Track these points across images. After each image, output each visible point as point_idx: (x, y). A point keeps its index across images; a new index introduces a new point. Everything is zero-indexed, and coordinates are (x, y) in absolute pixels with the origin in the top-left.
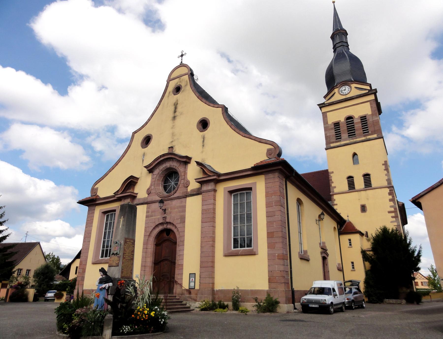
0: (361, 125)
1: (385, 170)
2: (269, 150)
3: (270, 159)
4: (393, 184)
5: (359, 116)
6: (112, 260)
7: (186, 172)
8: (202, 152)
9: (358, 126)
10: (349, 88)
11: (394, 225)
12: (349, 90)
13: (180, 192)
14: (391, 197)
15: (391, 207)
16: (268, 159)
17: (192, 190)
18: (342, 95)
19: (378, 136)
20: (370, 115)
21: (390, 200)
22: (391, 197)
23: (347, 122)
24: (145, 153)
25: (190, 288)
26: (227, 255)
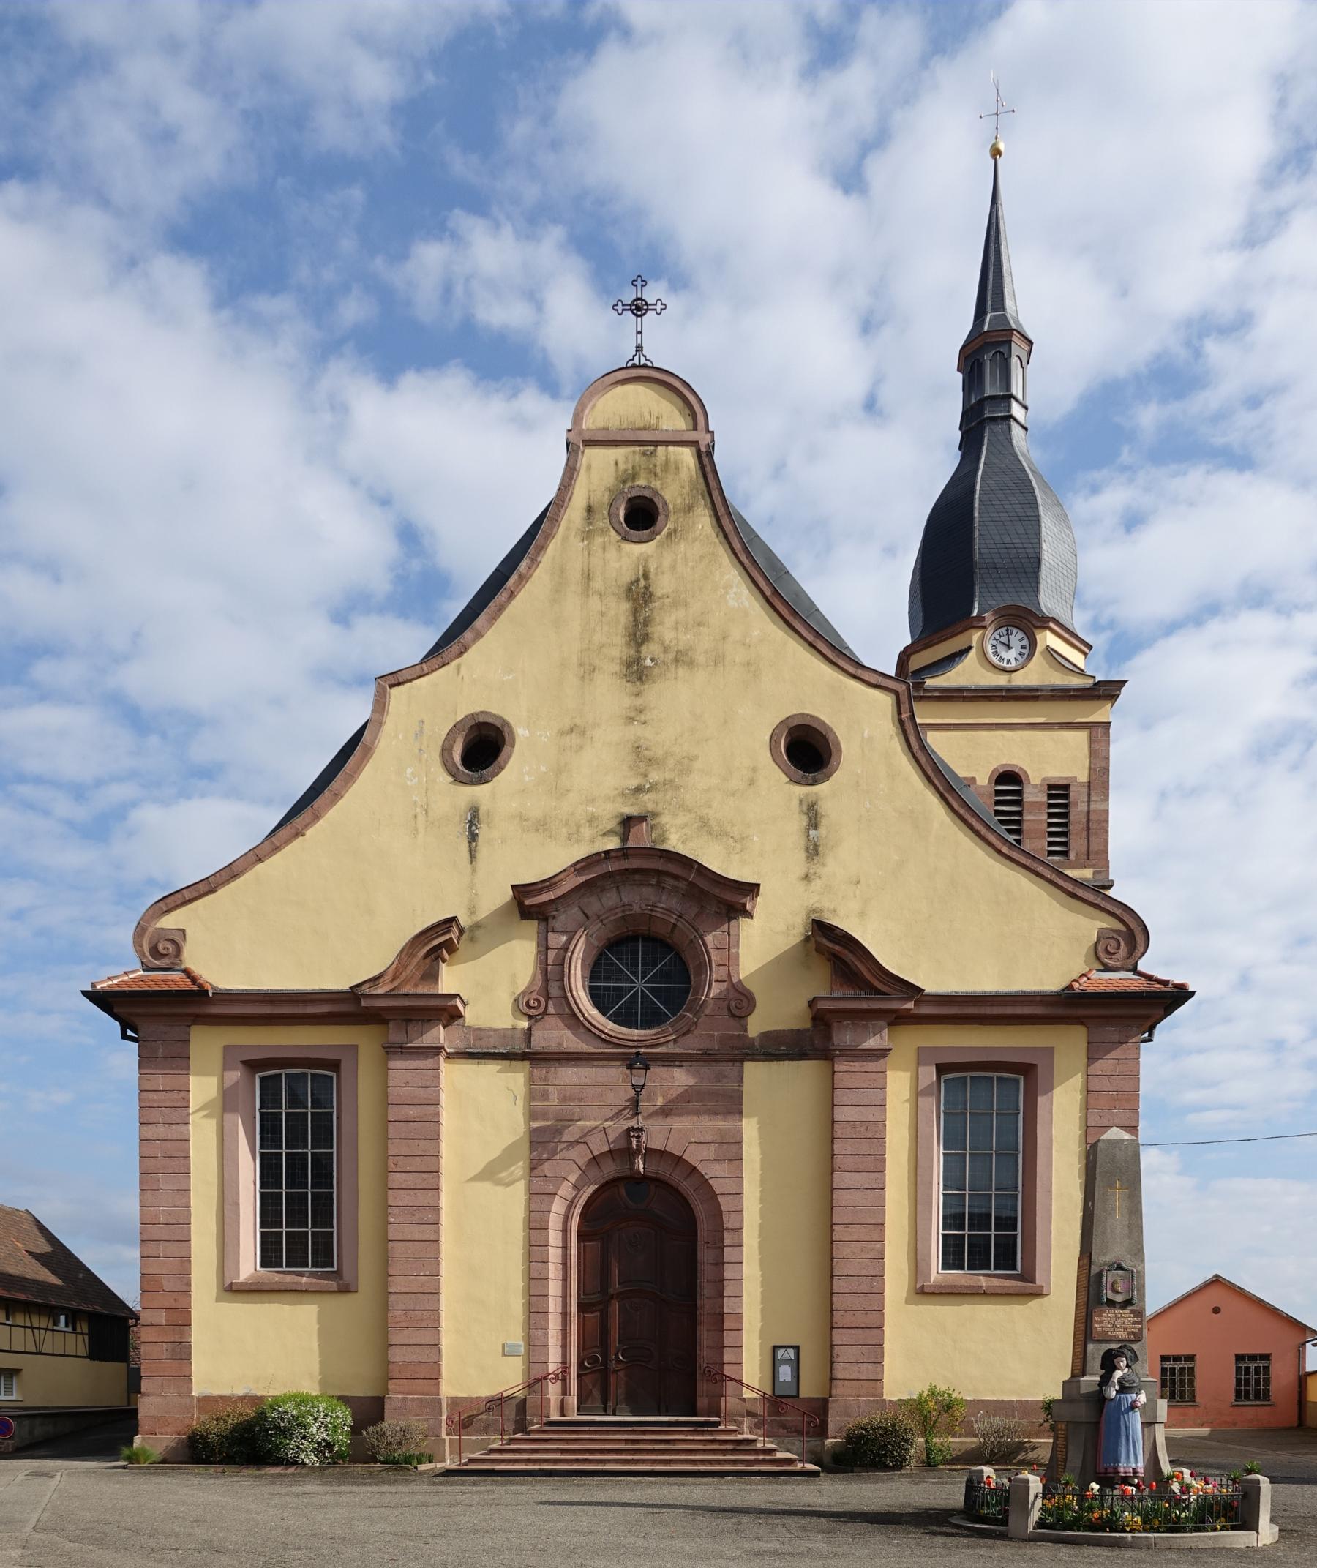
0: (1045, 817)
2: (1102, 935)
3: (1107, 969)
5: (1044, 779)
7: (733, 950)
8: (806, 877)
9: (1036, 819)
10: (1025, 642)
12: (1023, 651)
13: (713, 1036)
17: (766, 1036)
18: (995, 667)
19: (1099, 877)
20: (1081, 785)
23: (998, 793)
24: (482, 811)
26: (923, 1292)
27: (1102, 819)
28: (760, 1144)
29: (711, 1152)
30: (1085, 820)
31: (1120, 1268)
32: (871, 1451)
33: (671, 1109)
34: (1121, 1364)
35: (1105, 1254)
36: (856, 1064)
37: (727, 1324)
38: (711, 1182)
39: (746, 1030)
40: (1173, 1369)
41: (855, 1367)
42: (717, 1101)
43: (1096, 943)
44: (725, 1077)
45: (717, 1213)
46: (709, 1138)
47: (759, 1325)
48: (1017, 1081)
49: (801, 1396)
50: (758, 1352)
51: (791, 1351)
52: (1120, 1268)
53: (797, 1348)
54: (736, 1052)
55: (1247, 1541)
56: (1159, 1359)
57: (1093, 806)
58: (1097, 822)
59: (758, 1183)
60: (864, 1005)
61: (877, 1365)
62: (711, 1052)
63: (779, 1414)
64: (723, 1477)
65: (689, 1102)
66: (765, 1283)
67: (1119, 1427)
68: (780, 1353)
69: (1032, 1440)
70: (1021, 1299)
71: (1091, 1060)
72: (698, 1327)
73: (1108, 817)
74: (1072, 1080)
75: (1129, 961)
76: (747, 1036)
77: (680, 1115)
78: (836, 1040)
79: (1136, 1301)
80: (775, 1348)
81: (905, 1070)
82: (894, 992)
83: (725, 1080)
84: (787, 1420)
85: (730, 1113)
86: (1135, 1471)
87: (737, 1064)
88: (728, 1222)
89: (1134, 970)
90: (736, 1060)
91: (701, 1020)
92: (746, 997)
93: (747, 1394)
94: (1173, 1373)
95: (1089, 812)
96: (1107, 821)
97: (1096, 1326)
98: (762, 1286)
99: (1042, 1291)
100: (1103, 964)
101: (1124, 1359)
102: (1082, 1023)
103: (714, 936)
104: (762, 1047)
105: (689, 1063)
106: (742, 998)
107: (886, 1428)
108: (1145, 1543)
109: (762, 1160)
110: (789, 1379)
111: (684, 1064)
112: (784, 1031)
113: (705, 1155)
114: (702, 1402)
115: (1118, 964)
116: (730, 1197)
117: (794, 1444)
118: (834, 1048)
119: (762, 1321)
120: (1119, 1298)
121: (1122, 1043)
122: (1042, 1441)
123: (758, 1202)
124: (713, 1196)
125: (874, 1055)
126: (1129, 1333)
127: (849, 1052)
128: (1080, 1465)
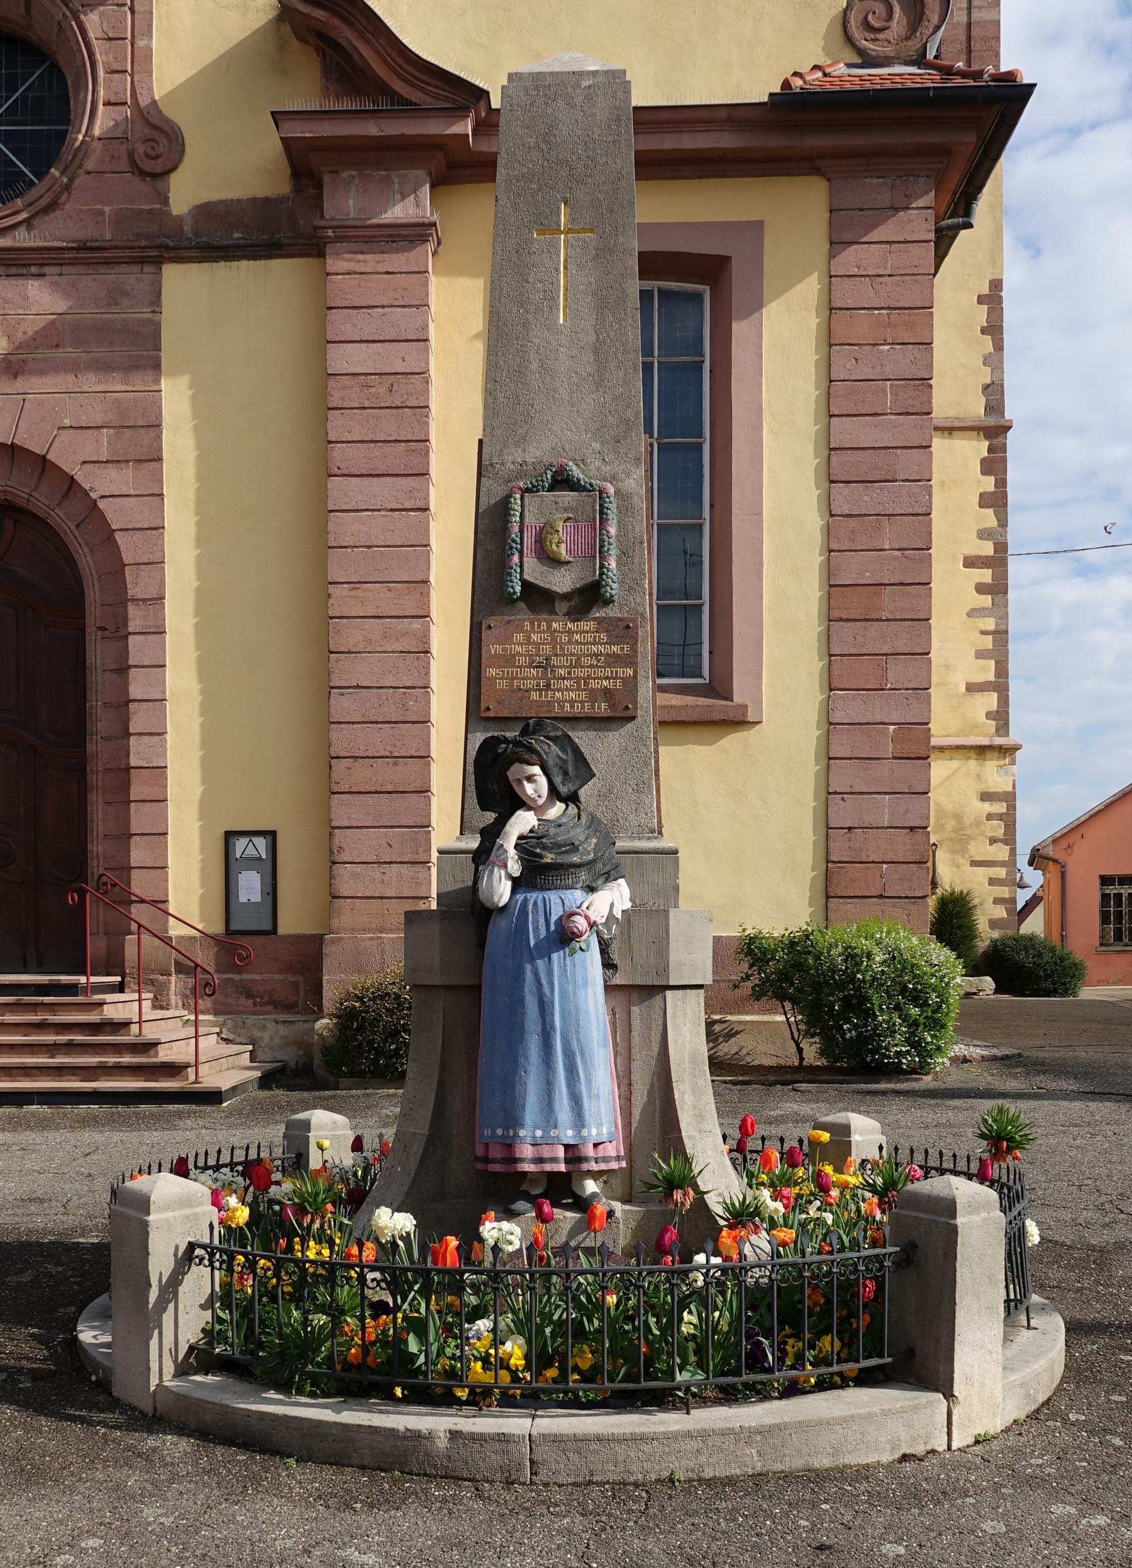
1: (984, 331)
3: (868, 61)
4: (1012, 411)
6: (522, 661)
7: (141, 43)
11: (983, 628)
13: (101, 213)
14: (989, 484)
15: (983, 534)
16: (859, 61)
17: (205, 212)
21: (985, 501)
22: (989, 484)
25: (233, 927)
27: (989, 34)
28: (196, 428)
29: (101, 445)
30: (963, 38)
31: (562, 481)
32: (371, 1043)
33: (24, 361)
34: (529, 788)
35: (522, 442)
36: (368, 257)
37: (137, 791)
38: (101, 505)
39: (165, 201)
40: (1119, 896)
41: (375, 872)
42: (111, 344)
43: (845, 12)
44: (126, 294)
45: (116, 569)
46: (98, 419)
47: (198, 790)
48: (698, 297)
49: (282, 930)
50: (196, 845)
51: (261, 843)
52: (562, 481)
53: (271, 835)
54: (144, 243)
55: (903, 1434)
56: (1098, 881)
57: (976, 15)
58: (982, 39)
59: (192, 507)
60: (371, 129)
61: (418, 867)
62: (94, 244)
63: (238, 970)
64: (20, 1105)
65: (57, 346)
66: (207, 707)
67: (518, 1002)
68: (240, 845)
69: (729, 1018)
70: (705, 732)
71: (837, 244)
72: (90, 797)
73: (999, 33)
74: (799, 287)
75: (910, 43)
76: (169, 213)
77: (42, 372)
78: (329, 211)
79: (613, 588)
80: (230, 836)
81: (473, 274)
82: (428, 99)
83: (125, 302)
84: (252, 981)
85: (136, 367)
86: (573, 1154)
87: (148, 269)
88: (137, 585)
89: (920, 60)
90: (142, 261)
91: (77, 182)
92: (167, 135)
93: (176, 930)
94: (1119, 903)
95: (969, 25)
96: (998, 39)
97: (492, 672)
98: (203, 713)
99: (745, 714)
100: (861, 52)
101: (536, 770)
102: (817, 171)
103: (101, 14)
104: (196, 234)
105: (57, 269)
106: (157, 135)
107: (398, 997)
108: (496, 1459)
109: (199, 460)
110: (256, 898)
111: (47, 270)
112: (238, 200)
113: (90, 454)
114: (95, 946)
115: (889, 50)
116: (139, 534)
117: (264, 1027)
118: (323, 223)
119: (203, 783)
120: (562, 582)
121: (897, 210)
122: (748, 1018)
123: (192, 544)
124: (108, 536)
125: (404, 238)
126: (593, 695)
127: (352, 233)
128: (426, 1131)
